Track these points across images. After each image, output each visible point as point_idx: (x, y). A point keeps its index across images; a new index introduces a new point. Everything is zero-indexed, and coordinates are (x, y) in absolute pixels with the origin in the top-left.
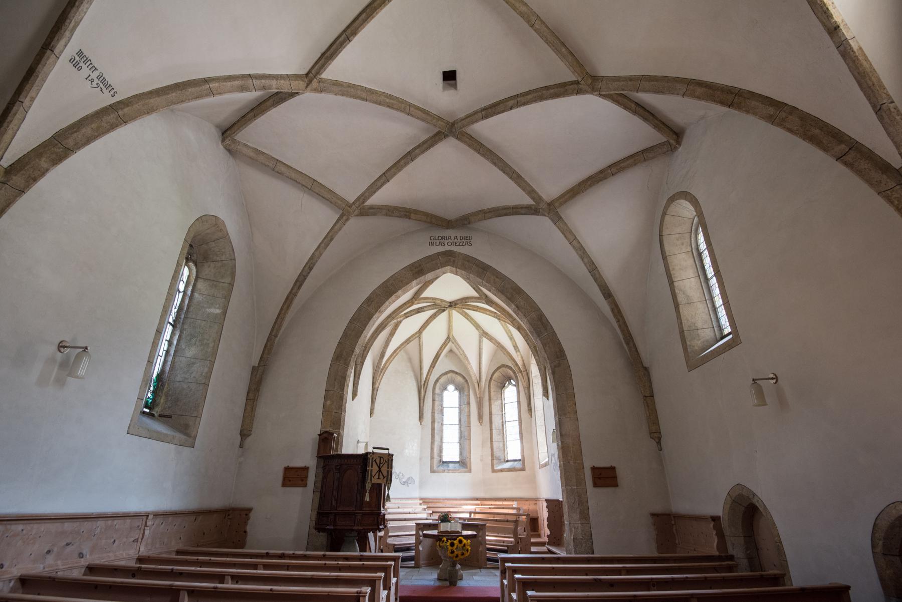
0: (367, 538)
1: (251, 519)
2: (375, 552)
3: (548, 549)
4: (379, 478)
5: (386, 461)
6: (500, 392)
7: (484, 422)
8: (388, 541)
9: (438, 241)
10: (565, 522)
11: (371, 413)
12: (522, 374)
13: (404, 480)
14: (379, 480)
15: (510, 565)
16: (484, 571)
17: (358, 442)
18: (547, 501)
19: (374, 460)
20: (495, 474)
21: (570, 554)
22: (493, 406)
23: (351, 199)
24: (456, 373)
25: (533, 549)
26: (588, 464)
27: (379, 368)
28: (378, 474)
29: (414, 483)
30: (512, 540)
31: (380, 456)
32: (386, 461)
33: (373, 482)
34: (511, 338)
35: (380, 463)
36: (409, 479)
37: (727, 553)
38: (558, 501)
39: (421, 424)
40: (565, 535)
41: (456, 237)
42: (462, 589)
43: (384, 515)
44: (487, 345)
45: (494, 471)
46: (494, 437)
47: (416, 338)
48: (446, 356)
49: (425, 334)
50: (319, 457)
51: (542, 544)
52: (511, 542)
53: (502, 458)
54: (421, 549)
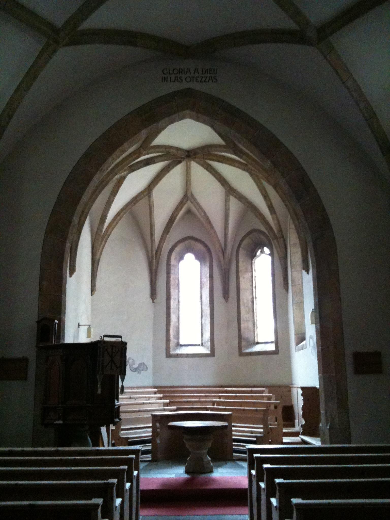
0: (100, 432)
2: (109, 446)
3: (302, 440)
4: (111, 369)
6: (250, 262)
7: (230, 299)
8: (120, 435)
9: (173, 76)
10: (322, 411)
11: (93, 290)
12: (278, 242)
13: (135, 366)
15: (259, 455)
16: (229, 464)
17: (79, 325)
18: (302, 388)
20: (242, 358)
21: (325, 444)
22: (241, 279)
23: (59, 22)
24: (196, 240)
25: (285, 440)
26: (349, 352)
27: (100, 235)
28: (110, 364)
29: (147, 370)
30: (262, 430)
34: (266, 197)
36: (140, 364)
38: (315, 388)
39: (153, 302)
40: (321, 425)
41: (196, 70)
42: (213, 481)
43: (119, 407)
44: (234, 204)
45: (241, 354)
46: (242, 315)
47: (144, 196)
48: (183, 218)
49: (156, 192)
50: (39, 348)
51: (296, 434)
52: (260, 433)
53: (251, 339)
54: (158, 441)
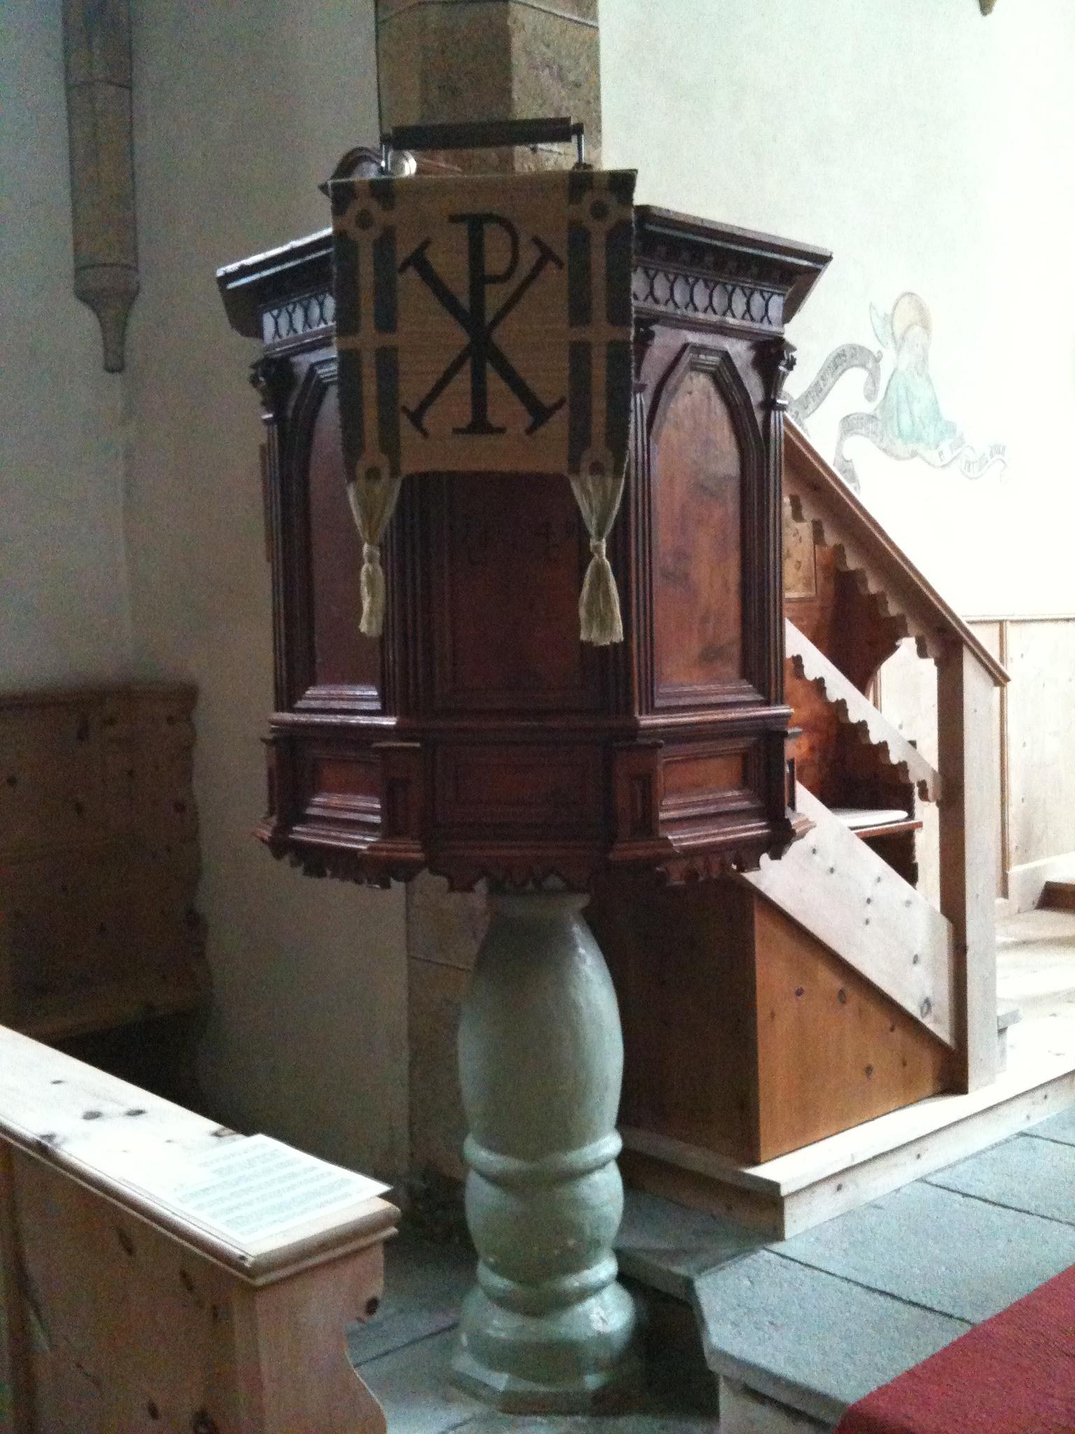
1: (834, 816)
4: (480, 425)
5: (546, 255)
14: (484, 441)
19: (404, 250)
28: (462, 382)
31: (481, 206)
32: (546, 255)
33: (407, 468)
35: (479, 280)
37: (804, 418)
